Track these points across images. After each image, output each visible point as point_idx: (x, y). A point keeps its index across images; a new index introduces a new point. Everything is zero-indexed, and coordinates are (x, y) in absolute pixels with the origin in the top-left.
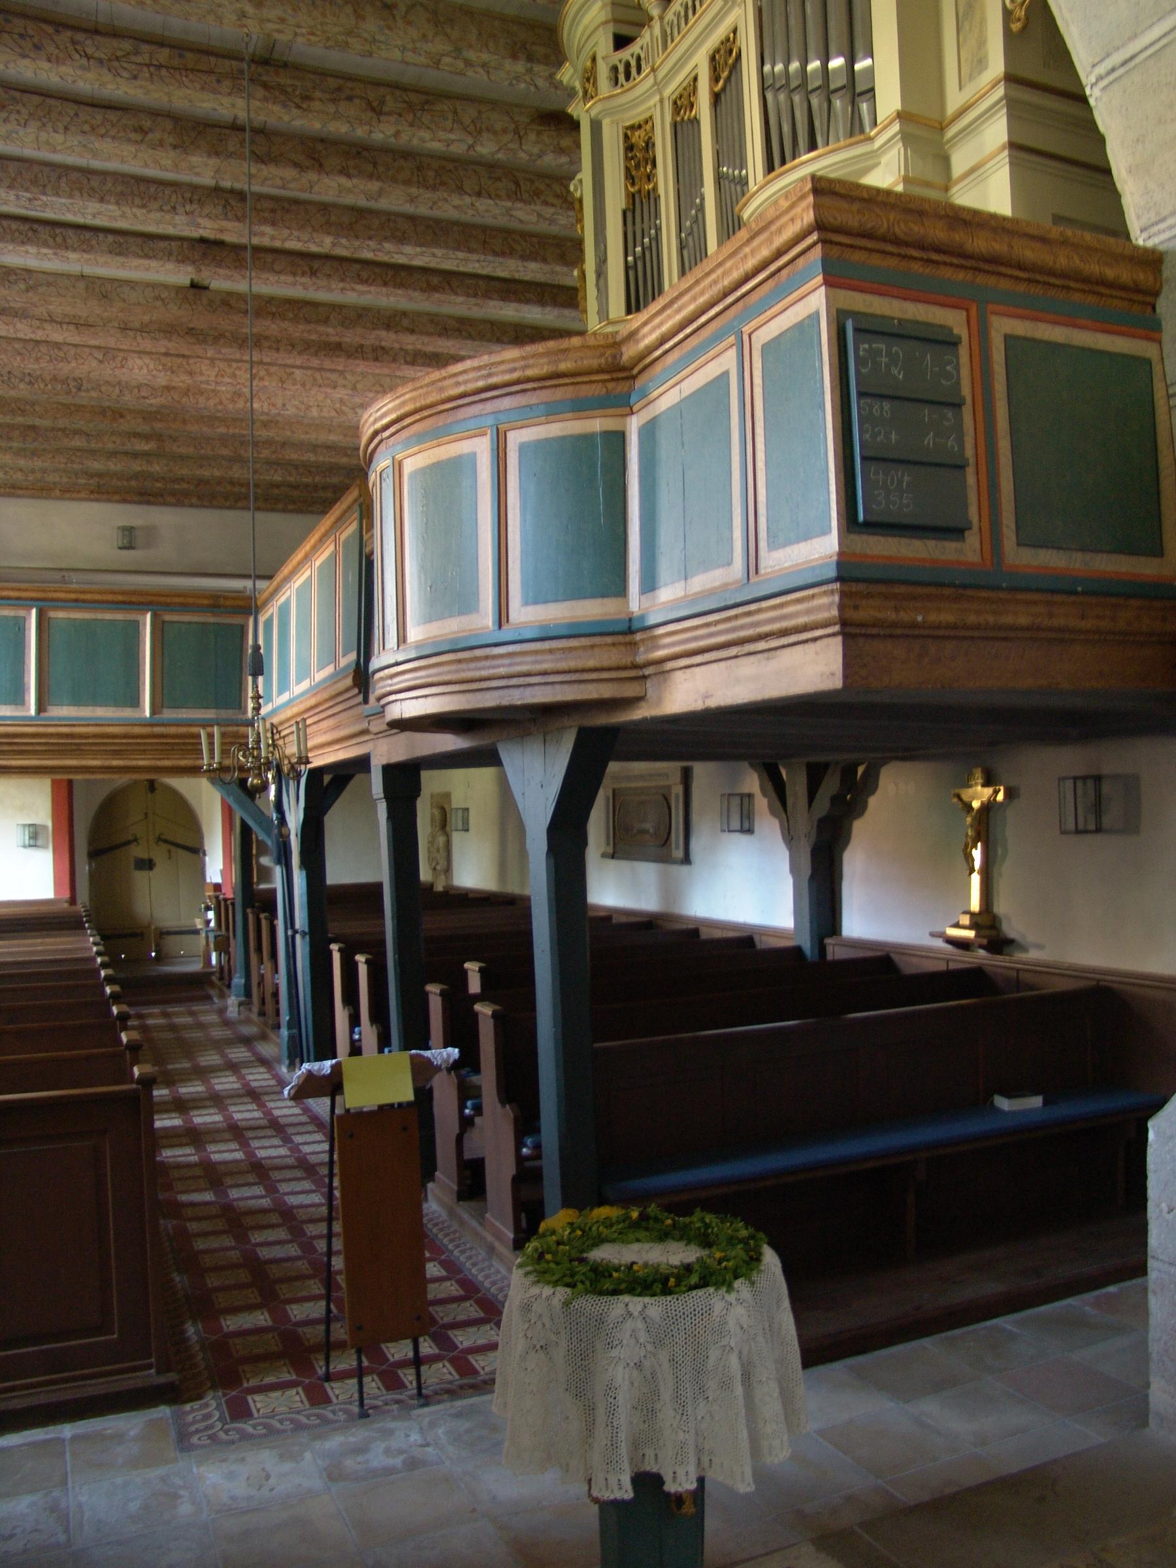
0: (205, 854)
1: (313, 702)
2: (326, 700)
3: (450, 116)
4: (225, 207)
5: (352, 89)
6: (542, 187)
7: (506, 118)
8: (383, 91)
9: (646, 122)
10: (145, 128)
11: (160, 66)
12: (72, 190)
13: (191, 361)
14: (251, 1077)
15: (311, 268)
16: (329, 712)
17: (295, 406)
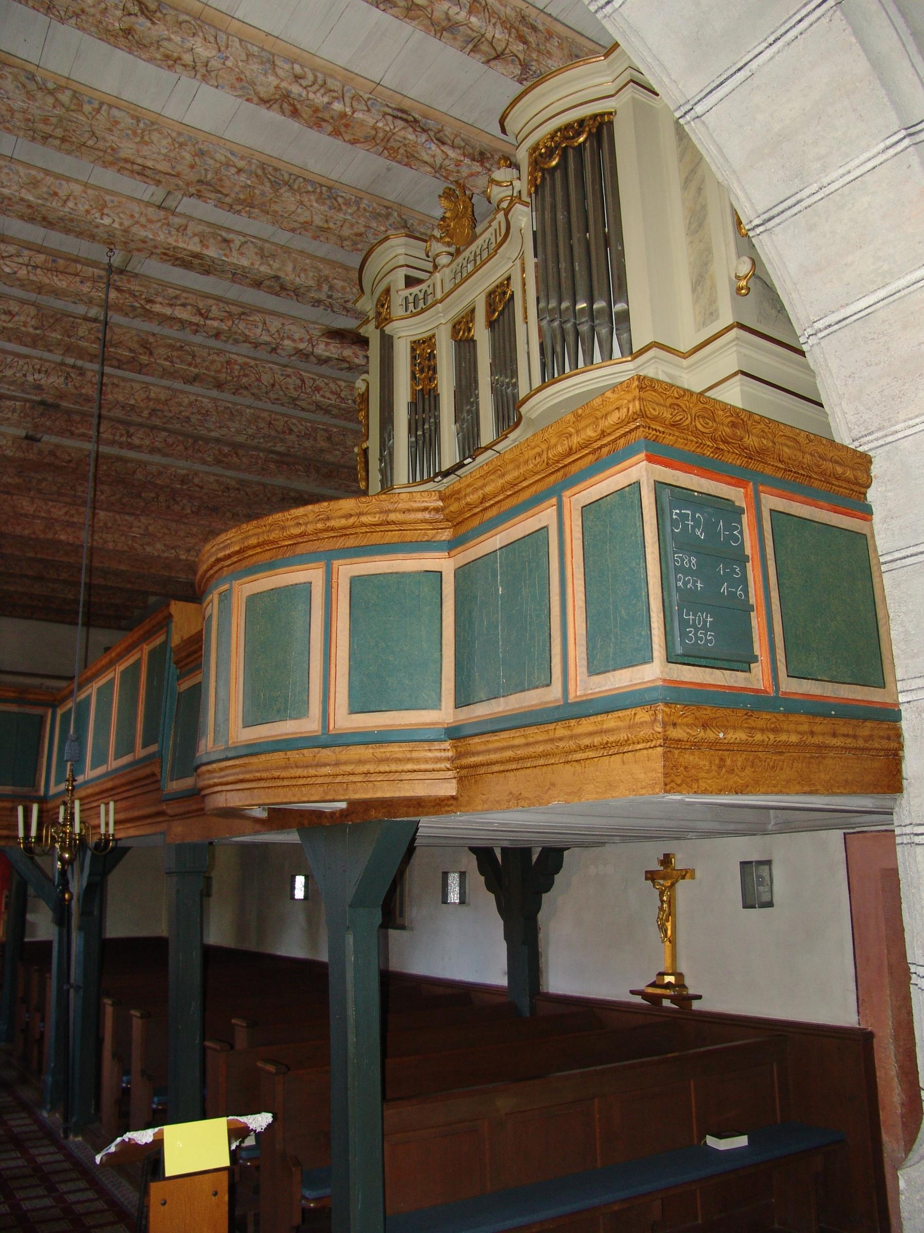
1: (110, 785)
2: (123, 785)
3: (260, 325)
4: (66, 378)
5: (186, 298)
6: (322, 385)
7: (303, 331)
8: (211, 302)
9: (430, 339)
10: (14, 313)
11: (36, 267)
14: (13, 1123)
15: (128, 432)
16: (125, 795)
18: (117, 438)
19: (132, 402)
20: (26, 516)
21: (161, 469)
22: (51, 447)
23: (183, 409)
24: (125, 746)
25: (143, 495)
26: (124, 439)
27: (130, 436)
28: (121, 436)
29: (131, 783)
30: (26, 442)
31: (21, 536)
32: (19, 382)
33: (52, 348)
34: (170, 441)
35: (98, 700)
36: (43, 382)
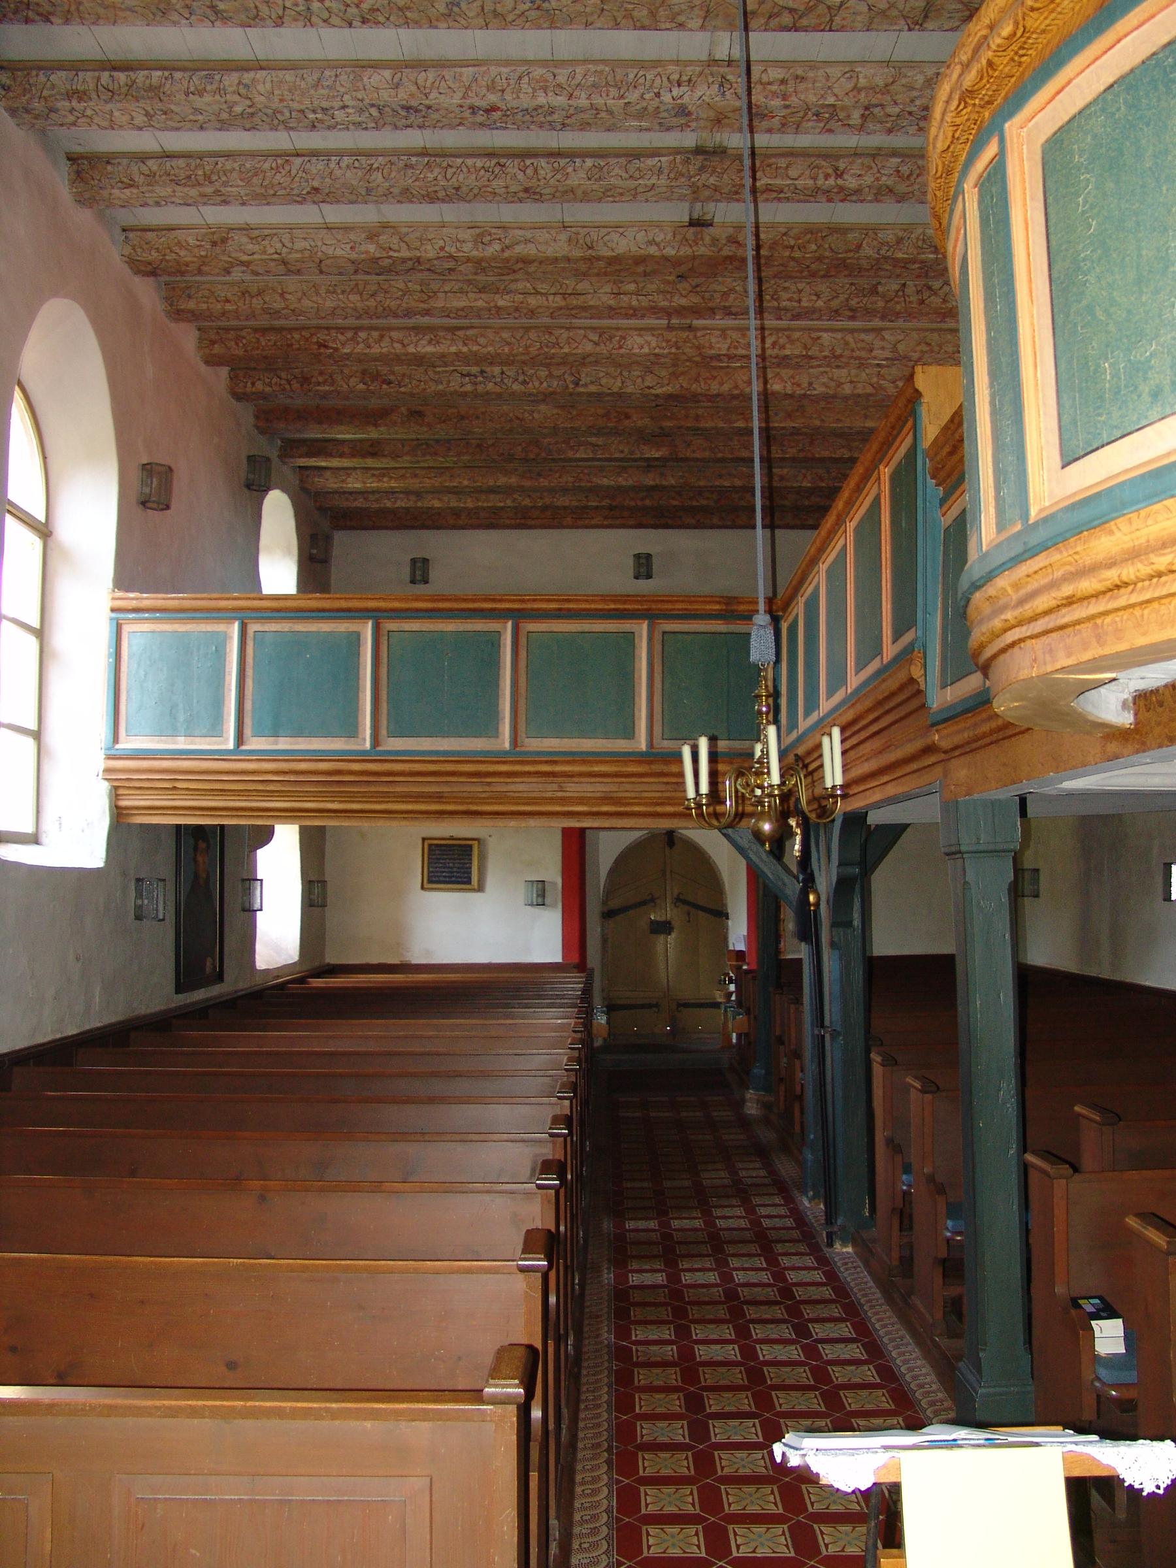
0: (727, 918)
2: (870, 710)
4: (721, 85)
12: (534, 90)
13: (699, 334)
15: (836, 169)
17: (824, 384)
18: (820, 182)
19: (831, 100)
20: (718, 357)
21: (900, 234)
22: (731, 230)
23: (915, 93)
24: (870, 646)
25: (880, 289)
26: (831, 181)
27: (839, 175)
28: (827, 176)
29: (880, 703)
30: (692, 230)
31: (718, 395)
32: (651, 109)
33: (681, 19)
34: (905, 170)
35: (828, 593)
36: (686, 99)
